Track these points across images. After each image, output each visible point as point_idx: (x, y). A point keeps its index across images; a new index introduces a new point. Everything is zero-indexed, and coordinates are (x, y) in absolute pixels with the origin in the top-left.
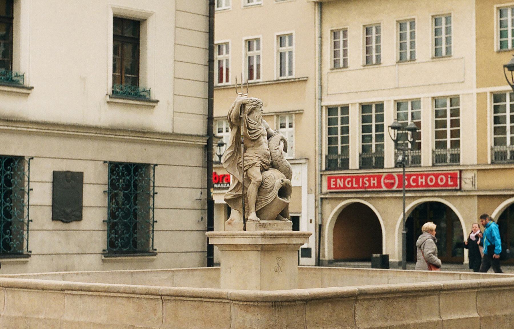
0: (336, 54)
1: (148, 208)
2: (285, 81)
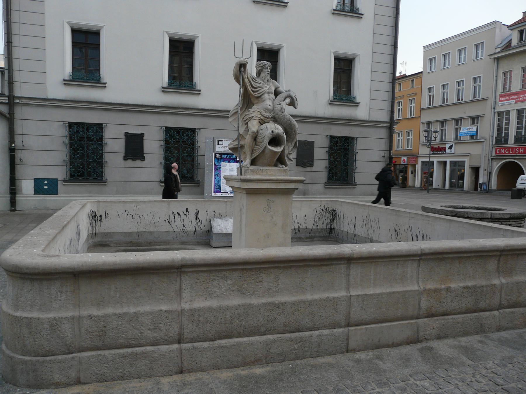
0: (505, 85)
1: (353, 161)
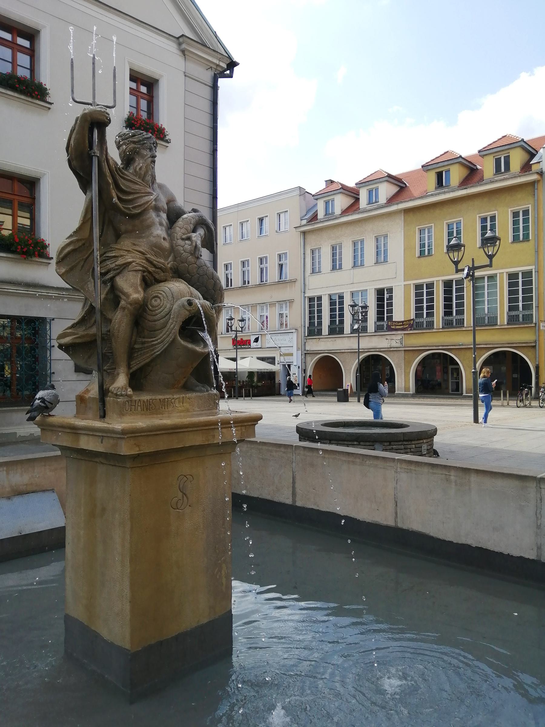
0: (313, 264)
2: (282, 282)
